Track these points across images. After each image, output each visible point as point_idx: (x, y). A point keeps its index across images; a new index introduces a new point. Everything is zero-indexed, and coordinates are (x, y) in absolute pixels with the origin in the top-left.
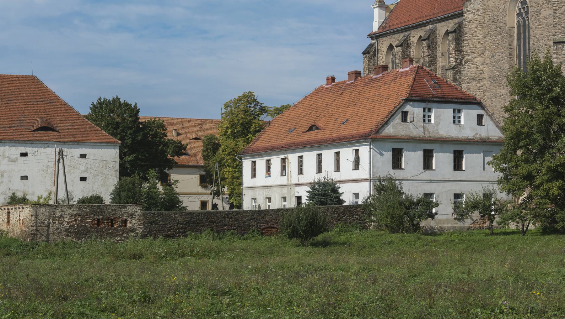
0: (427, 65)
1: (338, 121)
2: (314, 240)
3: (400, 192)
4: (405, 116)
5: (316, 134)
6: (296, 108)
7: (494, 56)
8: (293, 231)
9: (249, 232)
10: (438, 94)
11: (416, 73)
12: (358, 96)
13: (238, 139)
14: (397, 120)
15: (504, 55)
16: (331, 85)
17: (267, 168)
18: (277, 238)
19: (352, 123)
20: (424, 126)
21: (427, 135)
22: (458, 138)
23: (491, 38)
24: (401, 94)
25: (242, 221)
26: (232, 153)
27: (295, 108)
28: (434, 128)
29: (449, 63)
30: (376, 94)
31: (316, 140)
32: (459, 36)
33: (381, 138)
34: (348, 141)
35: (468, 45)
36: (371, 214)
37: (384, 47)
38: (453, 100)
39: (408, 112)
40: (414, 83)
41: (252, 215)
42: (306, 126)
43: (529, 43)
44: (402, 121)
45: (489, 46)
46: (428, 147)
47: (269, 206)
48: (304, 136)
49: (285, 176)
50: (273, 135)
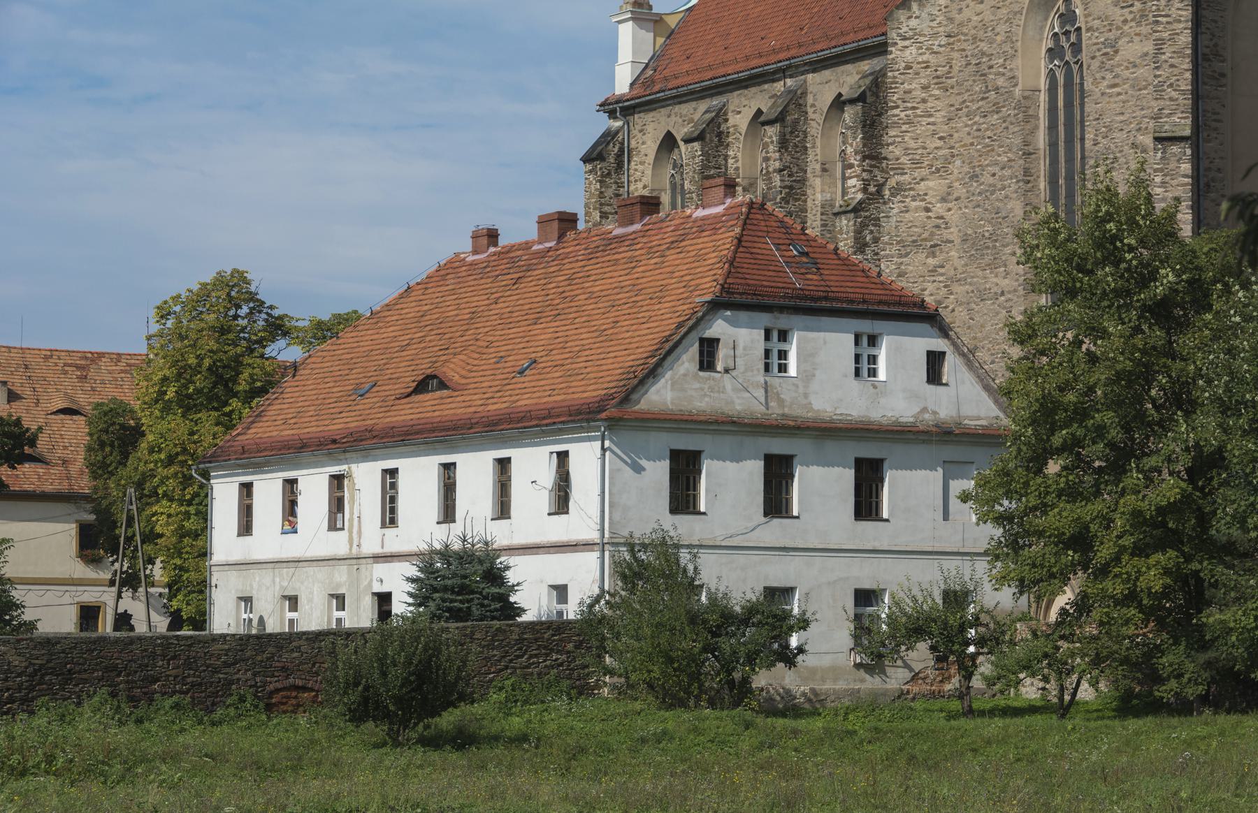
0: (778, 200)
1: (507, 365)
2: (427, 727)
3: (691, 583)
4: (708, 351)
5: (436, 402)
7: (977, 176)
8: (365, 700)
9: (229, 701)
10: (811, 288)
11: (745, 224)
12: (569, 288)
13: (199, 415)
14: (686, 365)
15: (1007, 172)
16: (486, 255)
17: (287, 504)
18: (314, 719)
20: (766, 383)
21: (775, 410)
22: (870, 423)
23: (970, 123)
24: (698, 285)
25: (208, 667)
26: (180, 458)
29: (844, 193)
30: (623, 284)
31: (439, 419)
34: (537, 426)
35: (900, 139)
36: (604, 648)
37: (649, 143)
38: (854, 307)
39: (718, 340)
42: (408, 379)
43: (1082, 139)
44: (702, 368)
45: (963, 146)
46: (779, 446)
48: (401, 407)
50: (307, 403)
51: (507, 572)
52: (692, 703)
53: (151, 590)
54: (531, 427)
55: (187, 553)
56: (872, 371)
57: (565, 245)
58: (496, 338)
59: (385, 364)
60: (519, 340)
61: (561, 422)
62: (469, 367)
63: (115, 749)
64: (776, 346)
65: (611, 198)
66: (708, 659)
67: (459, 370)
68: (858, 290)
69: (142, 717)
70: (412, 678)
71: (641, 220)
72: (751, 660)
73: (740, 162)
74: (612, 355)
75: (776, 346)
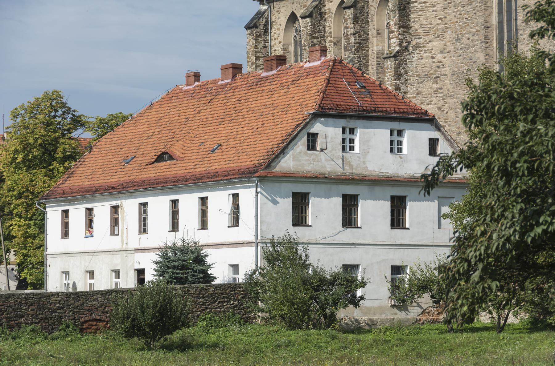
0: (353, 50)
1: (206, 147)
2: (165, 340)
3: (304, 263)
4: (312, 139)
5: (167, 167)
6: (135, 123)
7: (460, 39)
8: (133, 327)
9: (61, 327)
10: (367, 105)
11: (331, 71)
12: (238, 105)
13: (35, 171)
14: (301, 147)
15: (476, 38)
16: (193, 86)
17: (88, 221)
18: (106, 337)
19: (227, 150)
20: (343, 156)
21: (348, 171)
22: (398, 177)
23: (455, 10)
24: (306, 104)
25: (49, 309)
26: (25, 194)
27: (134, 122)
28: (359, 161)
29: (389, 46)
30: (267, 103)
31: (169, 176)
32: (405, 3)
33: (274, 177)
34: (221, 180)
35: (418, 19)
36: (258, 298)
37: (282, 18)
38: (390, 115)
39: (317, 134)
40: (326, 89)
41: (65, 299)
42: (152, 154)
43: (516, 19)
44: (309, 149)
45: (452, 23)
46: (350, 190)
47: (91, 285)
48: (149, 169)
49: (118, 235)
50: (98, 167)
51: (206, 258)
52: (304, 326)
53: (9, 267)
54: (218, 181)
55: (30, 246)
56: (399, 149)
57: (236, 81)
58: (199, 132)
59: (140, 146)
60: (212, 133)
61: (234, 178)
62: (185, 148)
63: (4, 353)
64: (348, 136)
65: (261, 49)
66: (312, 303)
67: (180, 149)
68: (392, 106)
69: (15, 336)
70: (157, 314)
71: (276, 68)
72: (335, 304)
73: (332, 29)
74: (261, 142)
75: (348, 136)
